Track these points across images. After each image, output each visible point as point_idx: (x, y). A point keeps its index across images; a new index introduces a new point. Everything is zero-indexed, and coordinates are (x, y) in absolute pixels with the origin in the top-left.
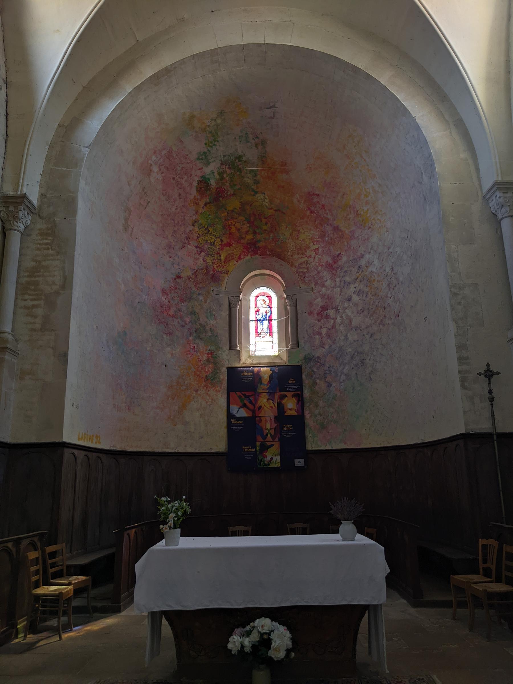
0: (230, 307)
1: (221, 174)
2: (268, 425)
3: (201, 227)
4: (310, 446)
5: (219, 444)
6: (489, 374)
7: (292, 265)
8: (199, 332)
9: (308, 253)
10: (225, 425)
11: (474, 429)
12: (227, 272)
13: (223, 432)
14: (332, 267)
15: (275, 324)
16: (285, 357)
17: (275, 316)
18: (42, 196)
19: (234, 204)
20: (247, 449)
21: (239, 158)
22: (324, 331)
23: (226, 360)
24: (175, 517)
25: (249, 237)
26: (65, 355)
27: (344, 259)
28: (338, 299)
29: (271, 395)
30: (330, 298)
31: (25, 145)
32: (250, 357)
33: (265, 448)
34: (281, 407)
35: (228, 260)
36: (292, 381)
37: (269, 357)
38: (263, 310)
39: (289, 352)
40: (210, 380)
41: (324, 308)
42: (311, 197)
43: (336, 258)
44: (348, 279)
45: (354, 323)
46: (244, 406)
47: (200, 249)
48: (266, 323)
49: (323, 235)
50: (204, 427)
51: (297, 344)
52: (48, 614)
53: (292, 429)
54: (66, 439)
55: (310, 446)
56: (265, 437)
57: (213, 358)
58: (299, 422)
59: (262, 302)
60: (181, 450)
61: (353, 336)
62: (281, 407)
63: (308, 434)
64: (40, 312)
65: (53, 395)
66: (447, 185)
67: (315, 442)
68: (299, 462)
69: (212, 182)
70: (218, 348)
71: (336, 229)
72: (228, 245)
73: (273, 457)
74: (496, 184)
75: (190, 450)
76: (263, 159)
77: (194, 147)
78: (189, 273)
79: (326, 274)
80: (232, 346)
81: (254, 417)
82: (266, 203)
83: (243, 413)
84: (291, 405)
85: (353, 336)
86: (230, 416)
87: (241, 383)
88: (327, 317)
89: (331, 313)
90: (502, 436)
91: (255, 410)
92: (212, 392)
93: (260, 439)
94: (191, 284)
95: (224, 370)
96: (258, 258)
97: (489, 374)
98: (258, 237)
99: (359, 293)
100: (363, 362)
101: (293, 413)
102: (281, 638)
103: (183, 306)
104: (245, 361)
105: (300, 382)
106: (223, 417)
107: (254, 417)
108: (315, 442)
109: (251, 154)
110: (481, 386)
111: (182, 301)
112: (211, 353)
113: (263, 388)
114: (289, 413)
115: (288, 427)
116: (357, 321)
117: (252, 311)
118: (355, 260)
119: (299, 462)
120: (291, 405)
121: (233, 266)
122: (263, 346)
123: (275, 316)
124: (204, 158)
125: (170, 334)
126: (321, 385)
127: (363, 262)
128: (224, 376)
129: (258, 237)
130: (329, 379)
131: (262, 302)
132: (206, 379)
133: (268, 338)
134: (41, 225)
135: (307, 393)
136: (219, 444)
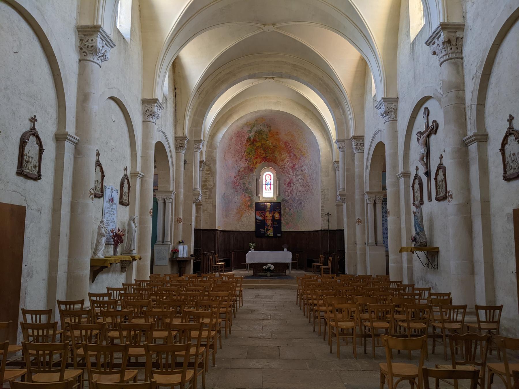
0: (257, 181)
1: (255, 136)
2: (269, 223)
3: (247, 152)
4: (283, 230)
5: (253, 228)
6: (328, 214)
7: (279, 166)
8: (246, 190)
9: (285, 162)
10: (254, 222)
11: (324, 228)
12: (256, 168)
13: (254, 224)
14: (293, 168)
15: (272, 186)
16: (275, 199)
17: (272, 183)
18: (206, 158)
19: (259, 144)
20: (262, 230)
21: (261, 130)
22: (289, 191)
23: (255, 200)
24: (168, 275)
25: (264, 155)
26: (215, 206)
27: (297, 166)
28: (294, 180)
29: (270, 212)
30: (291, 179)
31: (95, 4)
32: (263, 198)
33: (268, 230)
34: (273, 217)
35: (256, 163)
36: (278, 208)
37: (270, 198)
38: (268, 181)
39: (277, 197)
40: (250, 207)
41: (290, 183)
42: (286, 143)
43: (294, 165)
44: (298, 173)
45: (299, 190)
46: (261, 216)
47: (246, 160)
48: (269, 185)
49: (290, 156)
50: (248, 223)
51: (280, 195)
52: (216, 269)
53: (277, 224)
54: (217, 228)
55: (283, 230)
56: (268, 226)
57: (250, 199)
58: (279, 222)
59: (268, 177)
60: (241, 230)
61: (298, 194)
62: (273, 217)
63: (282, 226)
64: (208, 193)
65: (212, 216)
66: (323, 159)
67: (284, 228)
68: (279, 235)
69: (252, 138)
70: (252, 196)
71: (295, 155)
72: (256, 158)
73: (270, 233)
74: (383, 99)
75: (243, 230)
76: (270, 131)
77: (246, 129)
78: (243, 169)
79: (291, 170)
80: (257, 195)
81: (264, 220)
82: (270, 144)
83: (261, 218)
84: (277, 216)
85: (298, 194)
86: (256, 219)
87: (260, 208)
88: (290, 186)
89: (292, 185)
90: (330, 230)
91: (265, 217)
92: (250, 211)
93: (266, 227)
94: (243, 173)
95: (254, 203)
96: (267, 163)
97: (328, 214)
98: (267, 155)
99: (301, 179)
100: (301, 203)
101: (278, 219)
102: (272, 267)
103: (241, 181)
104: (261, 201)
105: (280, 208)
106: (254, 219)
107: (264, 220)
108: (284, 228)
109: (266, 129)
110: (326, 217)
111: (240, 179)
112: (250, 197)
113: (267, 210)
114: (276, 219)
115: (276, 223)
116: (300, 189)
117: (264, 181)
118: (301, 167)
119: (279, 235)
120: (277, 216)
121: (258, 165)
122: (268, 194)
123: (272, 183)
124: (250, 132)
125: (237, 192)
126: (287, 209)
127: (303, 168)
128: (254, 206)
129: (267, 155)
130: (290, 208)
131: (268, 177)
132: (248, 207)
133: (270, 191)
134: (206, 167)
135: (282, 212)
136: (253, 228)
